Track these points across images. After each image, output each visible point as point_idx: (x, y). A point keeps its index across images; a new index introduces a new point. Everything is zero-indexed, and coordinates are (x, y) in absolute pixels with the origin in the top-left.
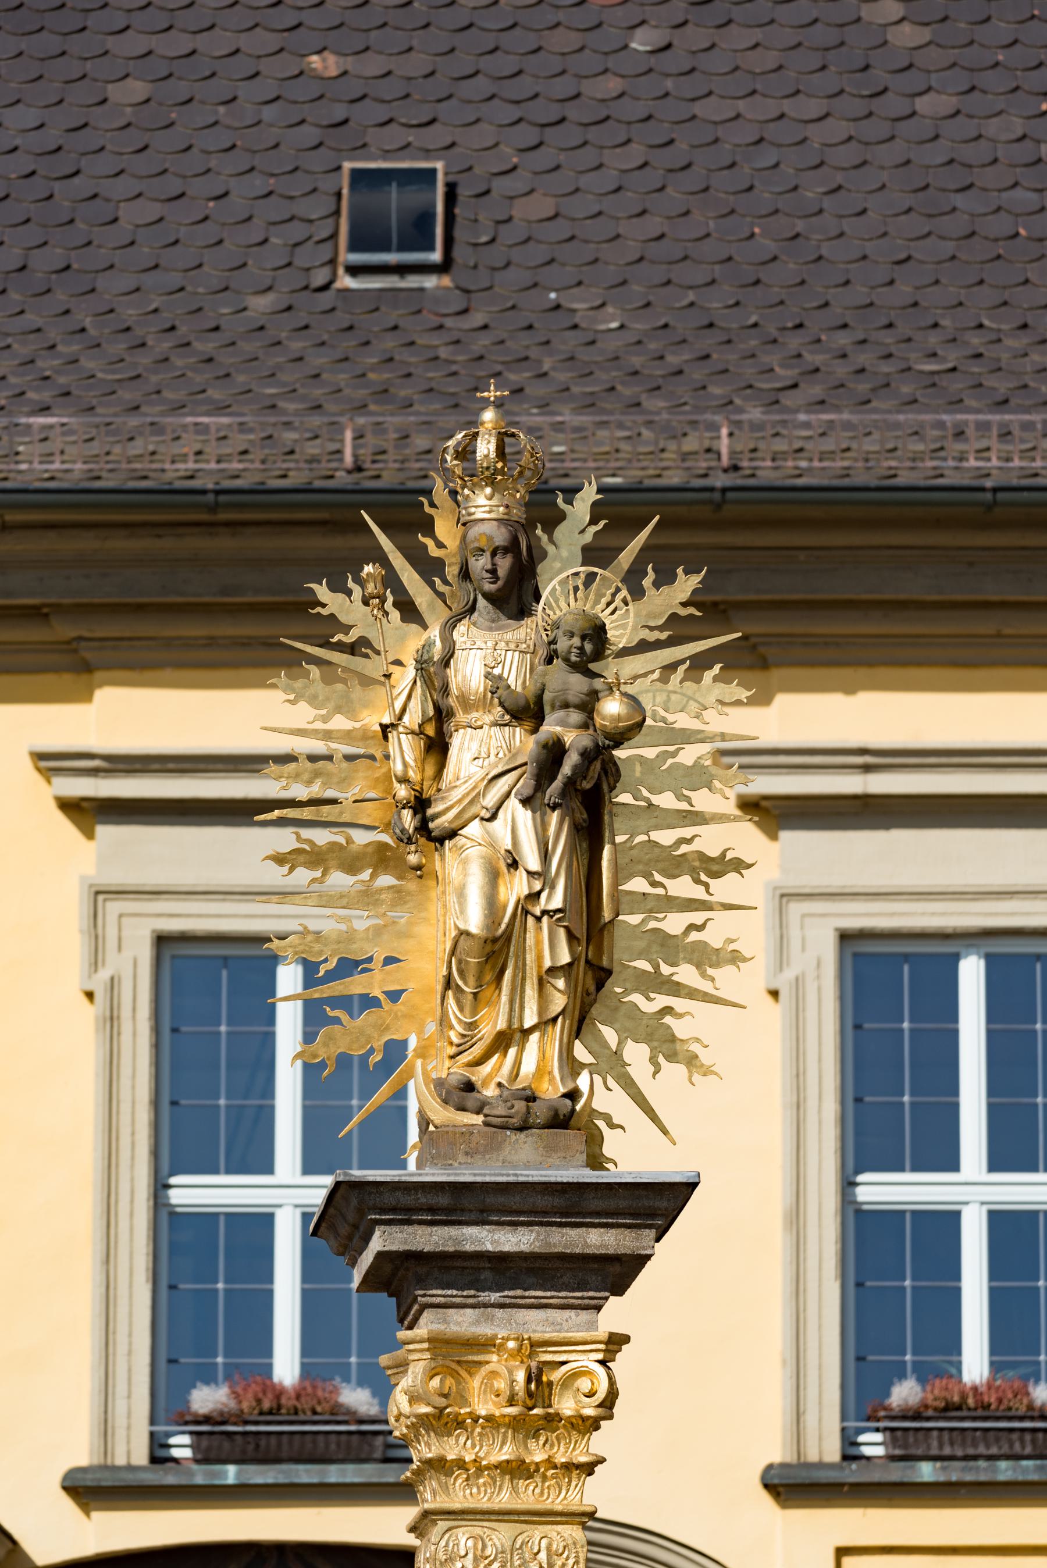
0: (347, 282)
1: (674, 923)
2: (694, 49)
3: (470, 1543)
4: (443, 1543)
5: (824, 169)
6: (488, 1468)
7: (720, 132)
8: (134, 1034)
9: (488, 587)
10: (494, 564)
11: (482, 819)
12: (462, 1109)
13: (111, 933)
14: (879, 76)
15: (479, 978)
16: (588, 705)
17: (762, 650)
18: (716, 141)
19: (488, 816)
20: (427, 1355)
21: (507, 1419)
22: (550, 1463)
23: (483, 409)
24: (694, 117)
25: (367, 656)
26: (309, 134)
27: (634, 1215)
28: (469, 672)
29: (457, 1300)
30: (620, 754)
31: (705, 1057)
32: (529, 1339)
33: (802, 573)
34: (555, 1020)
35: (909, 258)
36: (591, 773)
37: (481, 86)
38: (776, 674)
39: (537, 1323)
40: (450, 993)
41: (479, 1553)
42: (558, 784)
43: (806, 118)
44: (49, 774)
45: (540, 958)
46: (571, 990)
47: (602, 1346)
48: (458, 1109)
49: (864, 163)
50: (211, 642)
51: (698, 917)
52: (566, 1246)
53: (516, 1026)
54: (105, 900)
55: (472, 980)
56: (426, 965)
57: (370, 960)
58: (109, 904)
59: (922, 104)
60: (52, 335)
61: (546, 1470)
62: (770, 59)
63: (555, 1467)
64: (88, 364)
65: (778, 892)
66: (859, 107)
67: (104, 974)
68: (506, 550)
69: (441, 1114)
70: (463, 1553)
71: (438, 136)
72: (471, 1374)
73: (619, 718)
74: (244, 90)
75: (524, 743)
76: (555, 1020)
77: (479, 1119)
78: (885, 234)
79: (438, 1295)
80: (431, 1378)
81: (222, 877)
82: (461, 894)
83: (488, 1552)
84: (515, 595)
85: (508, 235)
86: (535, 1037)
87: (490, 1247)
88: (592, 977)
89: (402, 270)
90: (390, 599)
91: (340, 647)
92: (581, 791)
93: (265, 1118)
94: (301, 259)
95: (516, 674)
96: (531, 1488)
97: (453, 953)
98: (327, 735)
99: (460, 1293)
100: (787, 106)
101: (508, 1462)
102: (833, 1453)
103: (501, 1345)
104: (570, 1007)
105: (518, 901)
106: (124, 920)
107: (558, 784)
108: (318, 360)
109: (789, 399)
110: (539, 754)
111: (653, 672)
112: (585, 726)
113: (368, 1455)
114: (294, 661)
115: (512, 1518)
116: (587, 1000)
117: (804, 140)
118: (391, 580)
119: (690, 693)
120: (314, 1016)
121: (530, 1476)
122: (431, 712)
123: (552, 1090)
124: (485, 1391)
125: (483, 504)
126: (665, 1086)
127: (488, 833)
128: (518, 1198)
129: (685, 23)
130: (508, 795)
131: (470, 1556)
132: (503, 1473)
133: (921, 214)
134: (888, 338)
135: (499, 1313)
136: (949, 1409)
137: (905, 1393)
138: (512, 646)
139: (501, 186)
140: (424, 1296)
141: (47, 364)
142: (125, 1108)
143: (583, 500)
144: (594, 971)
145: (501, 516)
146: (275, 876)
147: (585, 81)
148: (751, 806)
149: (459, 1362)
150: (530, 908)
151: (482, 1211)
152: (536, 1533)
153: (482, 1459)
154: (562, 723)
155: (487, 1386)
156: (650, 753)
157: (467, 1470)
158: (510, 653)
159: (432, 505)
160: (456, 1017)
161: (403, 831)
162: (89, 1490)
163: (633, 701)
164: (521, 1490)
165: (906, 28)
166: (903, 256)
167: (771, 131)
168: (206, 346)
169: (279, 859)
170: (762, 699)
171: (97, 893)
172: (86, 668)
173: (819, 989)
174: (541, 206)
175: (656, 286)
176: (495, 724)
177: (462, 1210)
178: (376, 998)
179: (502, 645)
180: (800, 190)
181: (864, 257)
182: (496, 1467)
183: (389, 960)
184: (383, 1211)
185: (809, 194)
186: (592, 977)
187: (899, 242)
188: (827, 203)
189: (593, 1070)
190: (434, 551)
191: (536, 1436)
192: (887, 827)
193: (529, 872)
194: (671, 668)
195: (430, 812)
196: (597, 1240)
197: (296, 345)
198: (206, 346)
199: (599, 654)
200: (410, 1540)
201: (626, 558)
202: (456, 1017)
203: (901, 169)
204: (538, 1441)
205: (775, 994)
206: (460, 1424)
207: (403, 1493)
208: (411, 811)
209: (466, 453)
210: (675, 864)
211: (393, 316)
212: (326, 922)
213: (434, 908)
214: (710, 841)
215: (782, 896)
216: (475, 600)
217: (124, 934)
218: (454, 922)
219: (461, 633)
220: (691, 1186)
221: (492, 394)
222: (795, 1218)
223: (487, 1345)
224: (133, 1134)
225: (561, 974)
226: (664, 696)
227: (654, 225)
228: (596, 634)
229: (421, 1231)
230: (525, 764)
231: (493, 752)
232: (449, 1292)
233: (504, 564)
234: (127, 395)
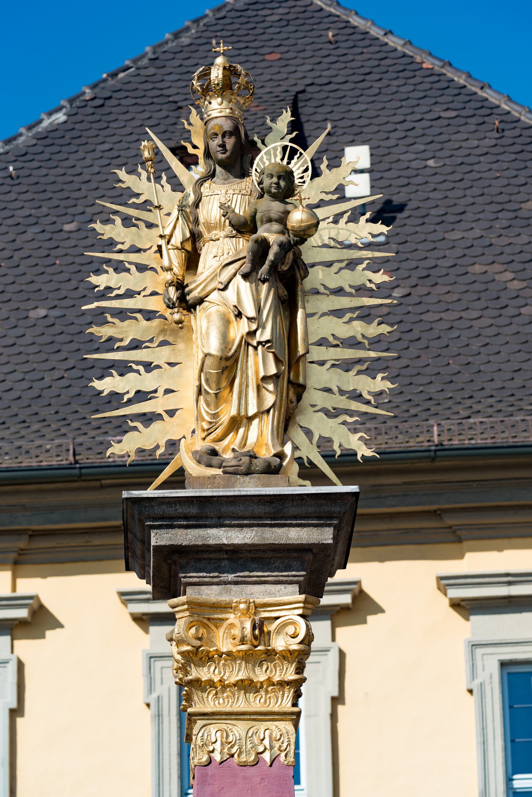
2: (421, 294)
3: (219, 734)
4: (200, 734)
5: (480, 337)
6: (229, 686)
7: (433, 325)
8: (170, 722)
9: (220, 156)
10: (223, 142)
11: (219, 289)
12: (210, 466)
13: (158, 676)
14: (504, 301)
15: (218, 383)
16: (283, 219)
17: (458, 532)
18: (432, 329)
19: (222, 287)
20: (187, 613)
21: (241, 654)
22: (269, 681)
23: (216, 57)
24: (421, 320)
25: (150, 211)
27: (318, 518)
28: (210, 212)
29: (207, 580)
32: (254, 602)
34: (268, 411)
35: (520, 369)
36: (287, 261)
38: (466, 544)
39: (260, 594)
40: (201, 398)
41: (224, 740)
42: (266, 267)
43: (472, 317)
45: (257, 373)
46: (278, 392)
47: (301, 605)
48: (207, 466)
49: (499, 334)
52: (275, 540)
53: (243, 414)
54: (155, 661)
55: (214, 385)
57: (155, 391)
58: (156, 663)
61: (268, 687)
62: (456, 297)
63: (274, 685)
65: (471, 644)
66: (496, 313)
67: (155, 695)
68: (231, 134)
70: (214, 740)
72: (217, 627)
73: (302, 221)
75: (243, 245)
76: (268, 411)
77: (219, 472)
78: (509, 361)
79: (194, 576)
80: (190, 628)
83: (230, 739)
84: (237, 159)
86: (256, 422)
87: (225, 542)
90: (164, 178)
95: (241, 209)
96: (258, 699)
97: (201, 370)
99: (208, 575)
100: (463, 314)
101: (242, 681)
103: (236, 607)
104: (278, 400)
105: (243, 337)
106: (164, 670)
107: (266, 267)
110: (253, 247)
111: (328, 218)
112: (282, 233)
115: (246, 717)
116: (291, 406)
117: (471, 327)
119: (352, 229)
121: (257, 691)
122: (188, 235)
124: (227, 638)
125: (217, 108)
127: (222, 297)
128: (242, 508)
129: (417, 285)
130: (235, 275)
131: (219, 742)
132: (240, 689)
133: (525, 352)
135: (234, 588)
138: (237, 192)
140: (185, 577)
142: (166, 757)
143: (282, 121)
144: (294, 388)
145: (228, 114)
147: (372, 310)
149: (209, 619)
150: (250, 341)
151: (219, 518)
152: (262, 726)
153: (225, 680)
154: (269, 231)
157: (216, 688)
158: (235, 196)
159: (190, 124)
160: (207, 412)
161: (169, 299)
164: (252, 700)
165: (515, 282)
166: (517, 368)
167: (456, 324)
170: (460, 556)
171: (151, 657)
173: (492, 688)
175: (405, 385)
176: (227, 237)
177: (207, 517)
178: (160, 415)
179: (231, 192)
180: (470, 346)
181: (500, 370)
182: (235, 685)
183: (168, 391)
184: (155, 519)
185: (474, 347)
187: (516, 363)
188: (482, 350)
191: (261, 665)
192: (521, 612)
193: (248, 318)
195: (187, 290)
202: (207, 412)
203: (515, 336)
204: (262, 668)
205: (471, 691)
206: (210, 659)
208: (174, 288)
215: (473, 645)
216: (215, 170)
217: (164, 676)
219: (205, 189)
221: (221, 49)
223: (226, 607)
224: (170, 769)
225: (270, 381)
226: (336, 231)
229: (181, 532)
230: (245, 257)
231: (226, 252)
232: (201, 574)
233: (230, 142)
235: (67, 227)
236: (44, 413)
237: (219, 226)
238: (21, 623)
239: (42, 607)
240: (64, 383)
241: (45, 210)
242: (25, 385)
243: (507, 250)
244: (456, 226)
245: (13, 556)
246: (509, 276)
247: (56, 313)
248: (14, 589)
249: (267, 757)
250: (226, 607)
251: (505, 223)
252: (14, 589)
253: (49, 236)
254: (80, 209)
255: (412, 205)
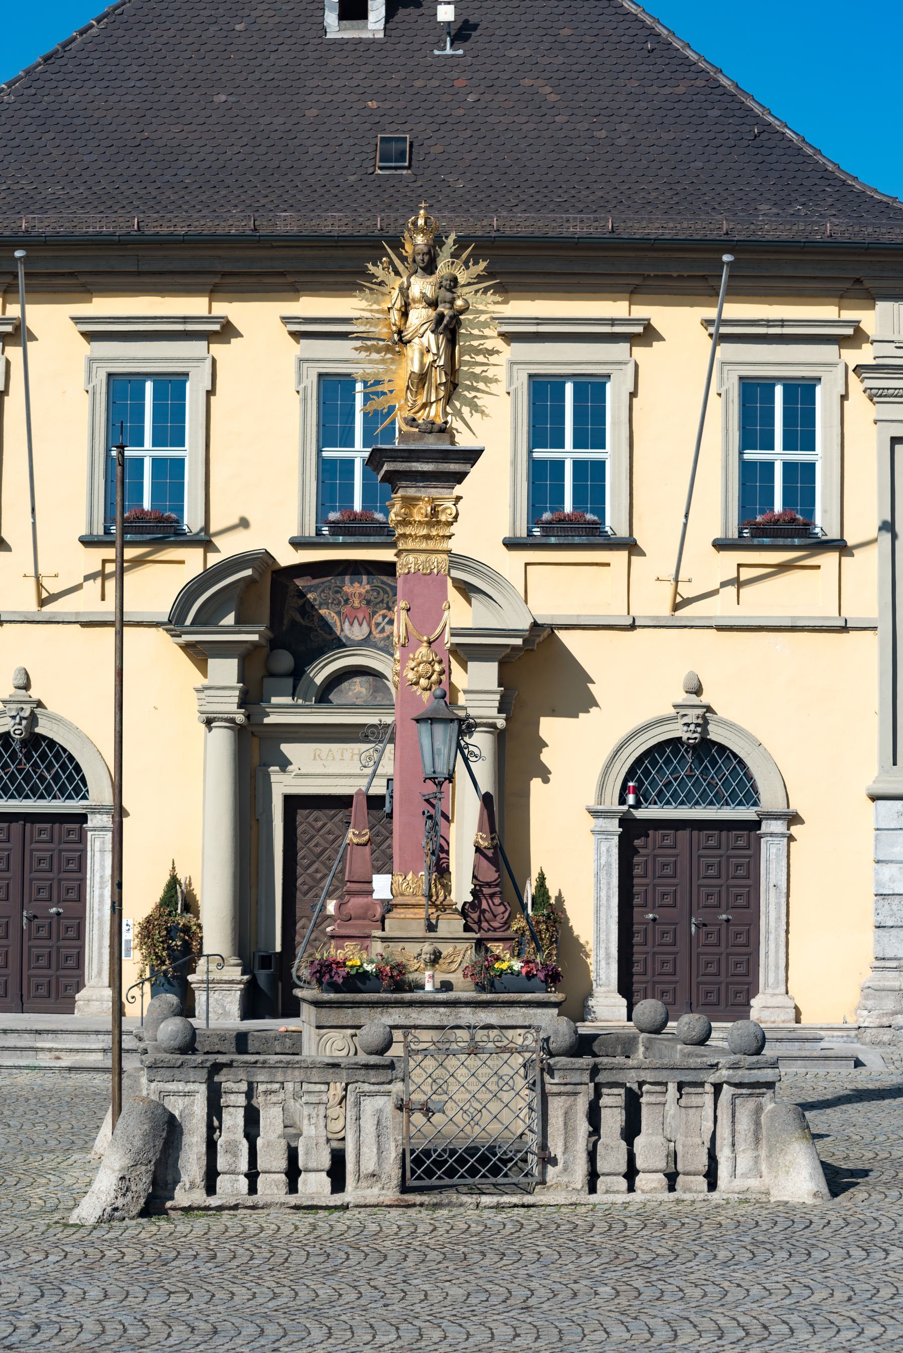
0: (379, 172)
1: (478, 370)
14: (544, 110)
16: (452, 302)
22: (438, 535)
26: (367, 126)
30: (461, 317)
31: (487, 411)
33: (517, 264)
37: (421, 112)
38: (510, 294)
39: (434, 492)
44: (286, 324)
46: (446, 390)
50: (336, 283)
51: (485, 368)
56: (401, 381)
59: (557, 119)
60: (288, 188)
62: (511, 104)
64: (298, 197)
66: (538, 119)
67: (302, 386)
69: (405, 428)
71: (407, 127)
74: (347, 112)
75: (431, 313)
79: (404, 484)
81: (339, 355)
82: (412, 360)
84: (429, 268)
85: (429, 158)
88: (452, 387)
89: (396, 168)
91: (375, 283)
92: (449, 328)
93: (352, 430)
94: (365, 164)
95: (430, 292)
98: (371, 311)
100: (515, 119)
102: (524, 534)
108: (370, 196)
109: (515, 209)
113: (384, 535)
114: (361, 288)
118: (391, 262)
120: (367, 398)
123: (440, 421)
125: (420, 239)
126: (475, 420)
134: (546, 191)
136: (560, 521)
137: (547, 516)
139: (427, 142)
141: (286, 197)
146: (355, 355)
148: (502, 335)
152: (433, 557)
155: (419, 512)
156: (471, 317)
162: (297, 544)
163: (466, 301)
168: (335, 191)
169: (356, 349)
170: (505, 302)
172: (298, 291)
174: (439, 149)
186: (452, 387)
189: (452, 415)
190: (404, 254)
194: (477, 291)
196: (453, 467)
197: (363, 191)
198: (335, 191)
199: (455, 286)
200: (395, 559)
201: (465, 255)
205: (509, 393)
207: (393, 545)
209: (415, 223)
210: (478, 352)
211: (392, 182)
212: (370, 369)
213: (404, 364)
214: (489, 344)
218: (410, 369)
219: (413, 279)
220: (483, 451)
221: (423, 205)
222: (514, 463)
223: (419, 499)
227: (473, 155)
228: (455, 280)
233: (426, 258)
234: (310, 206)
235: (238, 27)
236: (229, 181)
237: (419, 301)
238: (215, 333)
239: (229, 322)
240: (240, 157)
241: (221, 11)
242: (213, 157)
243: (548, 68)
244: (513, 45)
245: (210, 287)
246: (548, 89)
247: (232, 99)
248: (210, 312)
249: (435, 571)
250: (419, 499)
251: (548, 46)
252: (210, 312)
253: (225, 34)
254: (246, 12)
255: (483, 25)
